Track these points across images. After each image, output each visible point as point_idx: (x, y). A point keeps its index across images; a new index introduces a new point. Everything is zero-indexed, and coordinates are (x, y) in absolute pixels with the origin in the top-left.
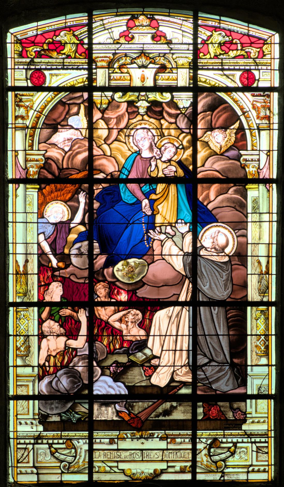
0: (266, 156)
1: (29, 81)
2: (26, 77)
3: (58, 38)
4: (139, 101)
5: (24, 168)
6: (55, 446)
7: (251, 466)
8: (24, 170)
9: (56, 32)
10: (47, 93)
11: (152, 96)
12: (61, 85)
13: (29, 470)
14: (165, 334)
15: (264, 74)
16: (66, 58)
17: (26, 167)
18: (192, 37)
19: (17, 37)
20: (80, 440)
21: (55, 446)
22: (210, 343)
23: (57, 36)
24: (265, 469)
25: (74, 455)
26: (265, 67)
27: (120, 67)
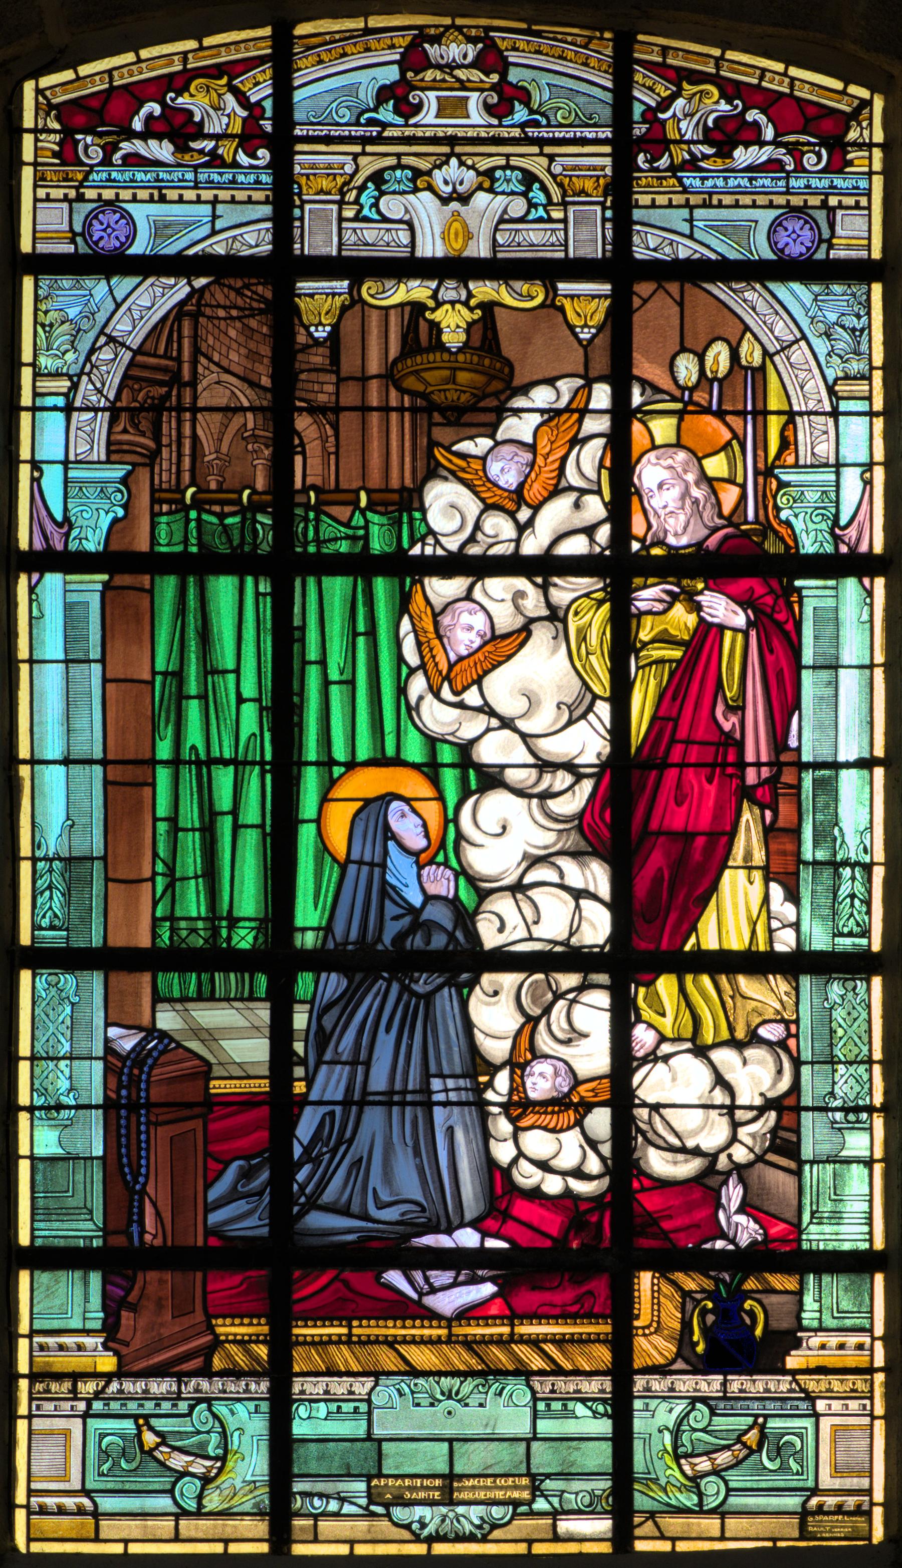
0: (860, 485)
1: (79, 239)
2: (71, 230)
3: (180, 100)
4: (439, 305)
5: (59, 517)
6: (160, 1424)
7: (815, 1491)
8: (60, 525)
9: (180, 82)
10: (138, 280)
11: (483, 290)
12: (191, 252)
13: (70, 1502)
14: (368, 1110)
15: (846, 218)
16: (205, 165)
17: (66, 519)
18: (608, 97)
19: (45, 97)
20: (238, 1406)
21: (160, 1424)
22: (374, 1189)
23: (179, 93)
24: (859, 1506)
25: (220, 1452)
26: (850, 201)
27: (673, 169)
